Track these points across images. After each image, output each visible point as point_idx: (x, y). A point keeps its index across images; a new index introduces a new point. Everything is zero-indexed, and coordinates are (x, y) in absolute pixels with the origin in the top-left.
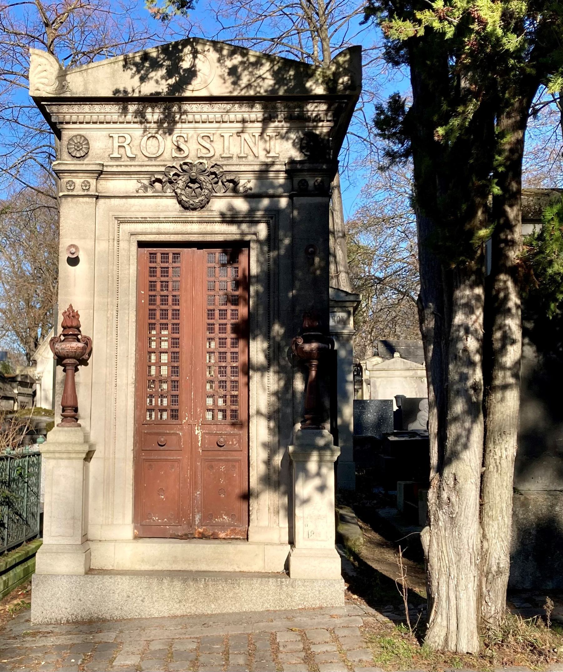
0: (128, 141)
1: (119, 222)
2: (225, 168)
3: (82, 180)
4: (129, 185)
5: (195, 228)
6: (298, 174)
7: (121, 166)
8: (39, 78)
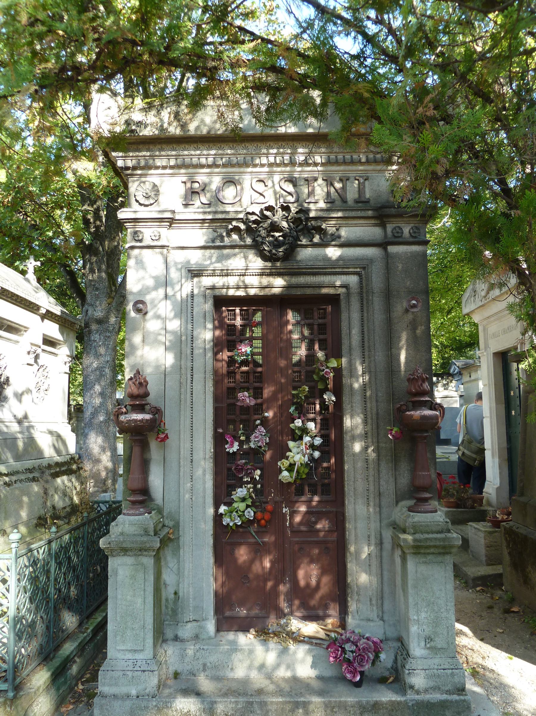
6: (392, 220)
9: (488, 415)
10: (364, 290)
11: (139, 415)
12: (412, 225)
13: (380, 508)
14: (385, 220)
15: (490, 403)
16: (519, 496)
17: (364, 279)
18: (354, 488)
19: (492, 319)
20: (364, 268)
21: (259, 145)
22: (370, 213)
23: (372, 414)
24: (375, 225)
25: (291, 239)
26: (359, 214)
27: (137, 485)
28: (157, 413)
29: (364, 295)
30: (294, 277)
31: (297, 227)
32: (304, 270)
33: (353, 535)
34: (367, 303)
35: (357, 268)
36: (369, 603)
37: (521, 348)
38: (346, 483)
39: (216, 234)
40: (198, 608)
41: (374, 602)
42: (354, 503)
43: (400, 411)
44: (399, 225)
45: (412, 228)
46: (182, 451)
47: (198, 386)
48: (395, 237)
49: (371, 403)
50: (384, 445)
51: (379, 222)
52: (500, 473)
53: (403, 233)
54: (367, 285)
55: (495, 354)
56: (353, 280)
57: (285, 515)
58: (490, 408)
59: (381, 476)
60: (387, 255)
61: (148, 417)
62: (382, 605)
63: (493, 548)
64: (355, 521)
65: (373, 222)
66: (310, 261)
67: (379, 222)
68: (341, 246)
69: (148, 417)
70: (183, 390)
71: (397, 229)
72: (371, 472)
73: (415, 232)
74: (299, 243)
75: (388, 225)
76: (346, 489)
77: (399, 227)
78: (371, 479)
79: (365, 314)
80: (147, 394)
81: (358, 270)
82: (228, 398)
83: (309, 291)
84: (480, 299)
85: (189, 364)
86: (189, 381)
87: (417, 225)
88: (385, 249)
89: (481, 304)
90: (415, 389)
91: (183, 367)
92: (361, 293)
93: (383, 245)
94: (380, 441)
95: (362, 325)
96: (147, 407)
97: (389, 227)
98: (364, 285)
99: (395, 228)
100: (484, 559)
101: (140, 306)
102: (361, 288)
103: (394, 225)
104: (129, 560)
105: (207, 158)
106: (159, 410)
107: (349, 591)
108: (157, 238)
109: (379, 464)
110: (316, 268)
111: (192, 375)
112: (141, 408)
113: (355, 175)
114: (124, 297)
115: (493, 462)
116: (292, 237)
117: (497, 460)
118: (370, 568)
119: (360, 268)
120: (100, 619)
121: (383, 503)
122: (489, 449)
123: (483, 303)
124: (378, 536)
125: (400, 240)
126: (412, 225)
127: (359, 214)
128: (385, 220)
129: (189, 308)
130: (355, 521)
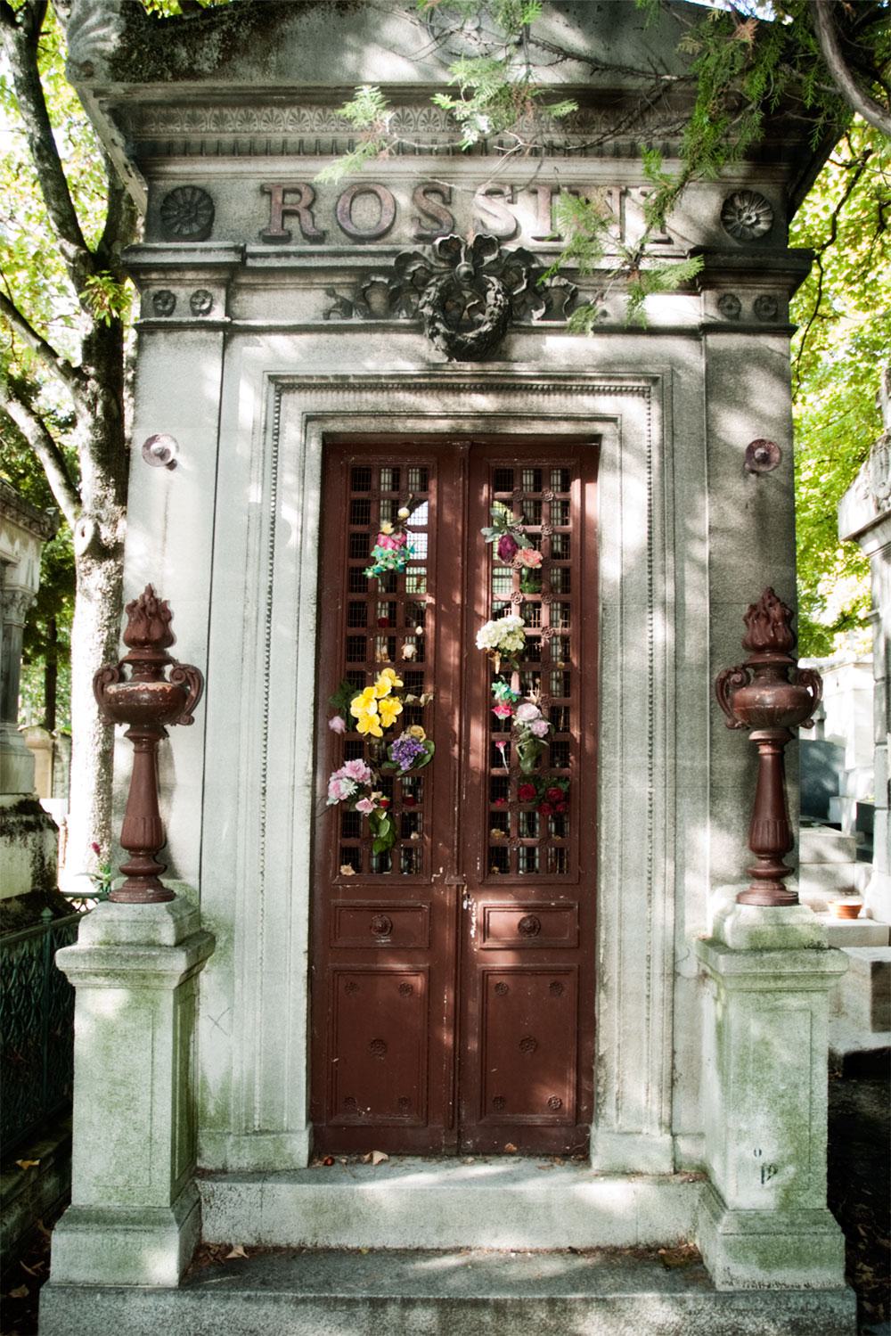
3: (192, 290)
4: (306, 303)
7: (287, 255)
23: (665, 694)
27: (141, 837)
33: (616, 956)
38: (603, 845)
39: (333, 302)
40: (318, 1208)
42: (620, 888)
46: (243, 768)
47: (283, 629)
50: (688, 763)
53: (740, 309)
68: (600, 330)
70: (248, 635)
72: (659, 822)
76: (603, 857)
77: (732, 295)
78: (658, 835)
82: (353, 522)
85: (265, 580)
86: (263, 618)
91: (250, 585)
104: (207, 1225)
111: (270, 604)
114: (787, 1191)
124: (669, 958)
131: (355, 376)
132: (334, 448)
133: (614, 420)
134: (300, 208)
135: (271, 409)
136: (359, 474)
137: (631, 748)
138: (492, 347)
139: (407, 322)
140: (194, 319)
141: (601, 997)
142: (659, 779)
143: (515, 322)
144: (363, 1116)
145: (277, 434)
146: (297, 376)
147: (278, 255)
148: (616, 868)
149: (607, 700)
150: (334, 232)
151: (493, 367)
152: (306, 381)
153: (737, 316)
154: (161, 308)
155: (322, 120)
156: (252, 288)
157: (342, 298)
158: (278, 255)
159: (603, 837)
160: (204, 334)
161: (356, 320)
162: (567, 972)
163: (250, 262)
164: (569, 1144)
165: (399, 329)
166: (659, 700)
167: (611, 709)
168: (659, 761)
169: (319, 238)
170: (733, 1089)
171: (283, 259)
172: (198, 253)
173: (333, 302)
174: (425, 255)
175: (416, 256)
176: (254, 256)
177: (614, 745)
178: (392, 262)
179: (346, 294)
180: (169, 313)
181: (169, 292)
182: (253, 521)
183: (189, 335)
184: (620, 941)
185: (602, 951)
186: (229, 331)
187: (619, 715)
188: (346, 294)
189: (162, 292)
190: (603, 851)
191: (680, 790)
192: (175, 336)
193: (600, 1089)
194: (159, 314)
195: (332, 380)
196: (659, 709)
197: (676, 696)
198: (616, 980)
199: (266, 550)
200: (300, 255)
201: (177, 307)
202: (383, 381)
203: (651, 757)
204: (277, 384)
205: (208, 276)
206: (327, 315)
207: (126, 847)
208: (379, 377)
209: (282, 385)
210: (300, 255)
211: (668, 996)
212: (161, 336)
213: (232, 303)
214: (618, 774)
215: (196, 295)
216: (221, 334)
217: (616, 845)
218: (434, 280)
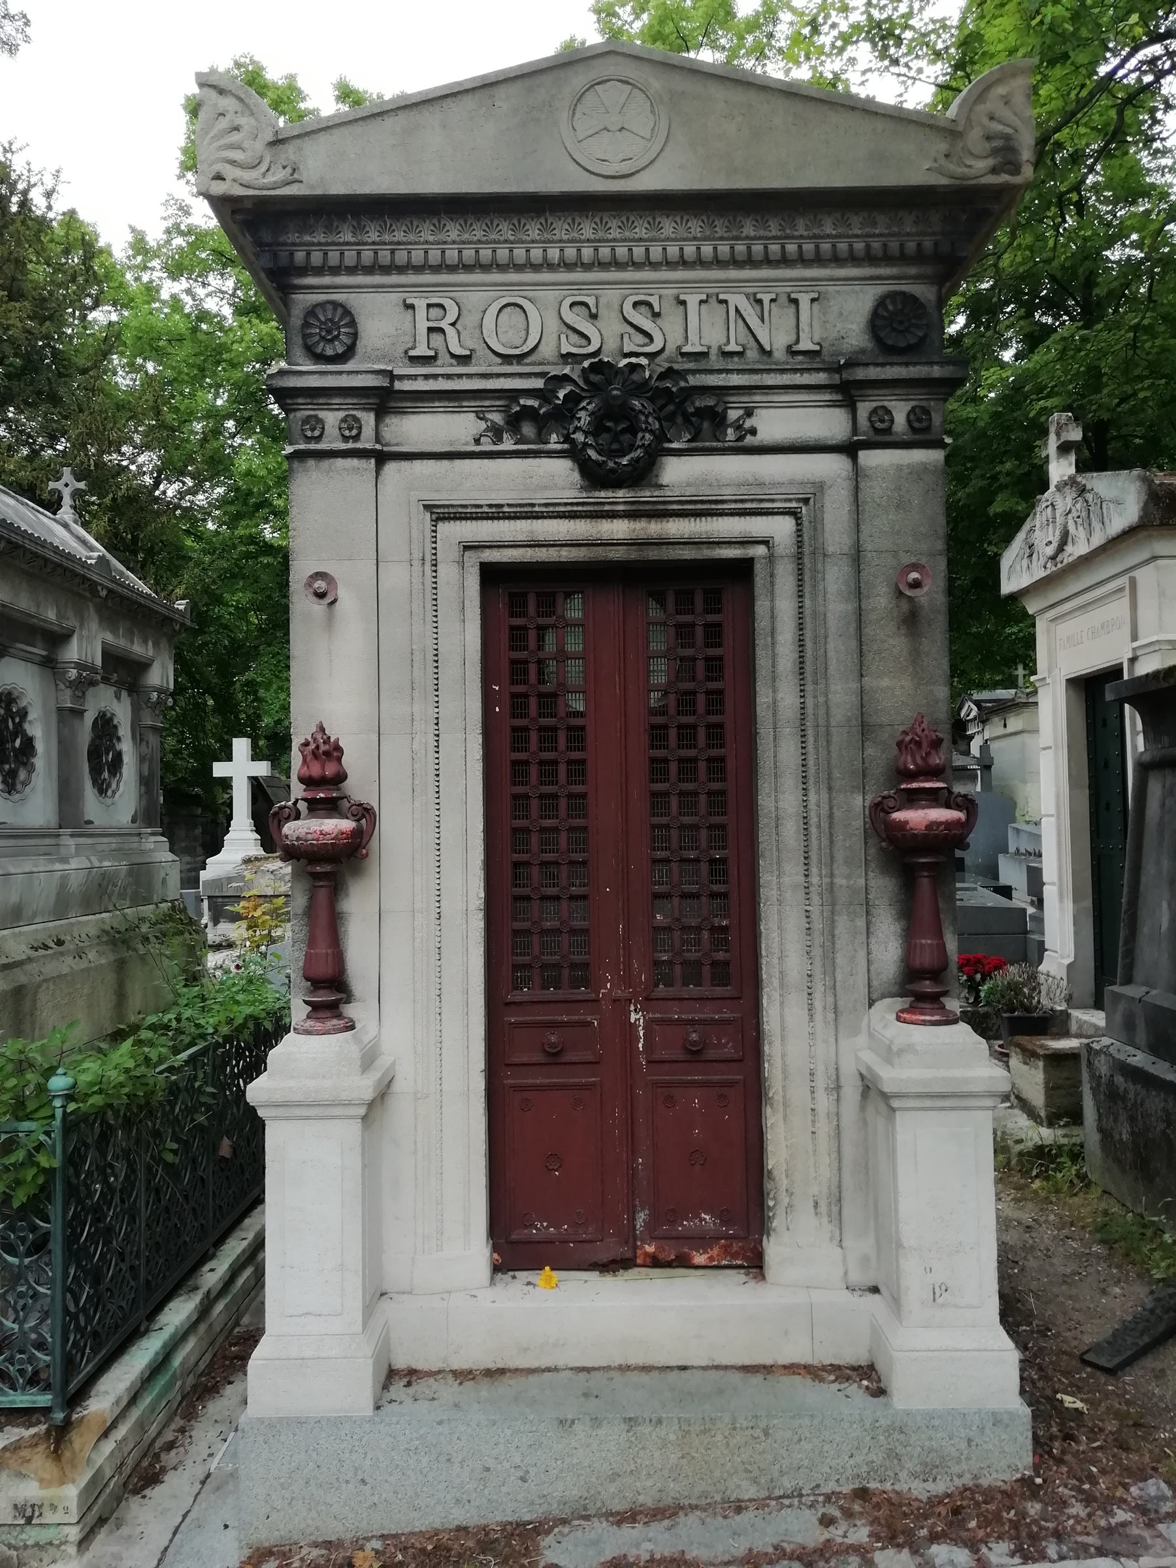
0: (452, 316)
1: (434, 517)
2: (693, 381)
3: (342, 414)
4: (460, 427)
5: (619, 529)
6: (870, 392)
7: (435, 377)
8: (221, 148)
9: (1053, 811)
10: (807, 550)
11: (327, 821)
12: (914, 403)
13: (835, 1013)
14: (853, 392)
15: (1057, 787)
16: (1122, 984)
17: (806, 523)
18: (781, 973)
19: (1067, 606)
20: (806, 501)
21: (415, 223)
22: (821, 378)
23: (819, 816)
24: (833, 404)
25: (647, 436)
26: (798, 379)
27: (324, 969)
28: (363, 816)
29: (806, 560)
30: (653, 521)
31: (661, 408)
32: (675, 507)
34: (813, 578)
35: (790, 500)
36: (812, 1210)
37: (1131, 670)
38: (764, 961)
39: (483, 425)
41: (823, 1208)
42: (782, 1003)
43: (879, 809)
44: (886, 404)
45: (913, 409)
48: (877, 431)
49: (818, 792)
50: (844, 882)
51: (839, 397)
52: (1076, 933)
53: (892, 421)
54: (814, 538)
55: (1073, 683)
56: (781, 529)
57: (633, 1027)
58: (1058, 797)
59: (837, 946)
60: (857, 473)
61: (347, 825)
62: (840, 1214)
63: (1063, 1092)
64: (783, 1039)
65: (827, 397)
66: (689, 485)
67: (839, 397)
69: (347, 825)
71: (880, 412)
72: (818, 939)
73: (919, 420)
74: (666, 445)
75: (860, 405)
77: (884, 407)
78: (817, 952)
79: (807, 602)
80: (341, 777)
81: (794, 505)
83: (688, 554)
84: (1042, 561)
85: (432, 712)
87: (924, 404)
88: (854, 458)
89: (1042, 574)
90: (915, 763)
92: (799, 557)
93: (849, 449)
94: (836, 872)
95: (801, 627)
96: (345, 804)
97: (864, 409)
98: (806, 538)
99: (874, 411)
100: (1043, 1114)
101: (320, 585)
102: (800, 544)
103: (875, 404)
105: (393, 252)
106: (367, 810)
107: (768, 1185)
108: (354, 432)
109: (833, 921)
110: (702, 502)
112: (331, 807)
113: (789, 289)
115: (1062, 909)
116: (651, 432)
117: (1069, 905)
118: (813, 1139)
119: (798, 500)
120: (251, 1236)
121: (840, 1003)
122: (1053, 884)
123: (1048, 572)
125: (887, 438)
126: (914, 403)
127: (798, 379)
128: (853, 392)
129: (429, 591)
130: (783, 1039)
131: (509, 505)
132: (491, 575)
133: (766, 542)
134: (444, 324)
135: (428, 540)
136: (516, 594)
137: (787, 867)
138: (642, 474)
139: (559, 447)
140: (344, 446)
141: (768, 1111)
142: (816, 899)
143: (666, 445)
144: (541, 1229)
145: (435, 565)
146: (452, 506)
147: (426, 377)
148: (776, 982)
149: (763, 821)
150: (481, 351)
151: (646, 495)
152: (461, 510)
153: (888, 431)
154: (309, 434)
155: (462, 231)
156: (402, 412)
157: (492, 421)
158: (426, 377)
159: (764, 953)
160: (354, 462)
161: (508, 445)
162: (731, 1084)
163: (398, 385)
164: (742, 1242)
165: (550, 454)
166: (813, 820)
167: (767, 830)
168: (815, 880)
169: (464, 360)
170: (1123, 1547)
171: (431, 381)
172: (344, 376)
173: (483, 425)
174: (575, 377)
175: (566, 378)
176: (401, 378)
177: (771, 864)
178: (539, 384)
179: (497, 418)
180: (318, 439)
181: (316, 417)
182: (416, 653)
183: (340, 462)
184: (783, 1056)
185: (766, 1065)
186: (382, 458)
187: (774, 836)
188: (497, 418)
189: (309, 416)
190: (764, 967)
191: (838, 908)
192: (326, 463)
193: (771, 1203)
194: (308, 439)
195: (486, 509)
196: (813, 830)
197: (831, 816)
198: (781, 1093)
199: (431, 682)
200: (449, 377)
201: (326, 432)
202: (537, 509)
203: (806, 876)
204: (432, 513)
205: (355, 401)
206: (477, 441)
207: (307, 979)
208: (533, 505)
209: (441, 514)
210: (449, 377)
211: (833, 1110)
212: (311, 463)
213: (381, 426)
214: (774, 892)
215: (344, 420)
216: (373, 461)
217: (776, 961)
218: (584, 404)
